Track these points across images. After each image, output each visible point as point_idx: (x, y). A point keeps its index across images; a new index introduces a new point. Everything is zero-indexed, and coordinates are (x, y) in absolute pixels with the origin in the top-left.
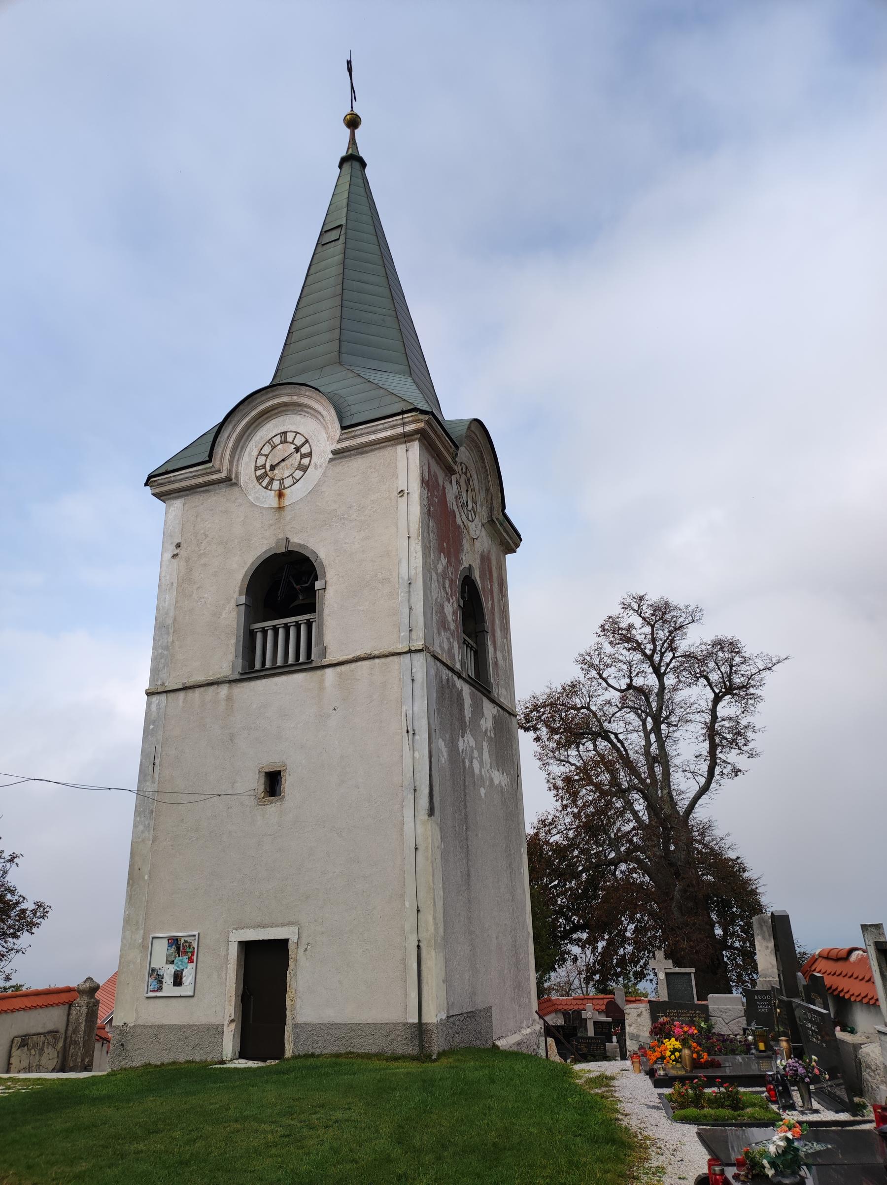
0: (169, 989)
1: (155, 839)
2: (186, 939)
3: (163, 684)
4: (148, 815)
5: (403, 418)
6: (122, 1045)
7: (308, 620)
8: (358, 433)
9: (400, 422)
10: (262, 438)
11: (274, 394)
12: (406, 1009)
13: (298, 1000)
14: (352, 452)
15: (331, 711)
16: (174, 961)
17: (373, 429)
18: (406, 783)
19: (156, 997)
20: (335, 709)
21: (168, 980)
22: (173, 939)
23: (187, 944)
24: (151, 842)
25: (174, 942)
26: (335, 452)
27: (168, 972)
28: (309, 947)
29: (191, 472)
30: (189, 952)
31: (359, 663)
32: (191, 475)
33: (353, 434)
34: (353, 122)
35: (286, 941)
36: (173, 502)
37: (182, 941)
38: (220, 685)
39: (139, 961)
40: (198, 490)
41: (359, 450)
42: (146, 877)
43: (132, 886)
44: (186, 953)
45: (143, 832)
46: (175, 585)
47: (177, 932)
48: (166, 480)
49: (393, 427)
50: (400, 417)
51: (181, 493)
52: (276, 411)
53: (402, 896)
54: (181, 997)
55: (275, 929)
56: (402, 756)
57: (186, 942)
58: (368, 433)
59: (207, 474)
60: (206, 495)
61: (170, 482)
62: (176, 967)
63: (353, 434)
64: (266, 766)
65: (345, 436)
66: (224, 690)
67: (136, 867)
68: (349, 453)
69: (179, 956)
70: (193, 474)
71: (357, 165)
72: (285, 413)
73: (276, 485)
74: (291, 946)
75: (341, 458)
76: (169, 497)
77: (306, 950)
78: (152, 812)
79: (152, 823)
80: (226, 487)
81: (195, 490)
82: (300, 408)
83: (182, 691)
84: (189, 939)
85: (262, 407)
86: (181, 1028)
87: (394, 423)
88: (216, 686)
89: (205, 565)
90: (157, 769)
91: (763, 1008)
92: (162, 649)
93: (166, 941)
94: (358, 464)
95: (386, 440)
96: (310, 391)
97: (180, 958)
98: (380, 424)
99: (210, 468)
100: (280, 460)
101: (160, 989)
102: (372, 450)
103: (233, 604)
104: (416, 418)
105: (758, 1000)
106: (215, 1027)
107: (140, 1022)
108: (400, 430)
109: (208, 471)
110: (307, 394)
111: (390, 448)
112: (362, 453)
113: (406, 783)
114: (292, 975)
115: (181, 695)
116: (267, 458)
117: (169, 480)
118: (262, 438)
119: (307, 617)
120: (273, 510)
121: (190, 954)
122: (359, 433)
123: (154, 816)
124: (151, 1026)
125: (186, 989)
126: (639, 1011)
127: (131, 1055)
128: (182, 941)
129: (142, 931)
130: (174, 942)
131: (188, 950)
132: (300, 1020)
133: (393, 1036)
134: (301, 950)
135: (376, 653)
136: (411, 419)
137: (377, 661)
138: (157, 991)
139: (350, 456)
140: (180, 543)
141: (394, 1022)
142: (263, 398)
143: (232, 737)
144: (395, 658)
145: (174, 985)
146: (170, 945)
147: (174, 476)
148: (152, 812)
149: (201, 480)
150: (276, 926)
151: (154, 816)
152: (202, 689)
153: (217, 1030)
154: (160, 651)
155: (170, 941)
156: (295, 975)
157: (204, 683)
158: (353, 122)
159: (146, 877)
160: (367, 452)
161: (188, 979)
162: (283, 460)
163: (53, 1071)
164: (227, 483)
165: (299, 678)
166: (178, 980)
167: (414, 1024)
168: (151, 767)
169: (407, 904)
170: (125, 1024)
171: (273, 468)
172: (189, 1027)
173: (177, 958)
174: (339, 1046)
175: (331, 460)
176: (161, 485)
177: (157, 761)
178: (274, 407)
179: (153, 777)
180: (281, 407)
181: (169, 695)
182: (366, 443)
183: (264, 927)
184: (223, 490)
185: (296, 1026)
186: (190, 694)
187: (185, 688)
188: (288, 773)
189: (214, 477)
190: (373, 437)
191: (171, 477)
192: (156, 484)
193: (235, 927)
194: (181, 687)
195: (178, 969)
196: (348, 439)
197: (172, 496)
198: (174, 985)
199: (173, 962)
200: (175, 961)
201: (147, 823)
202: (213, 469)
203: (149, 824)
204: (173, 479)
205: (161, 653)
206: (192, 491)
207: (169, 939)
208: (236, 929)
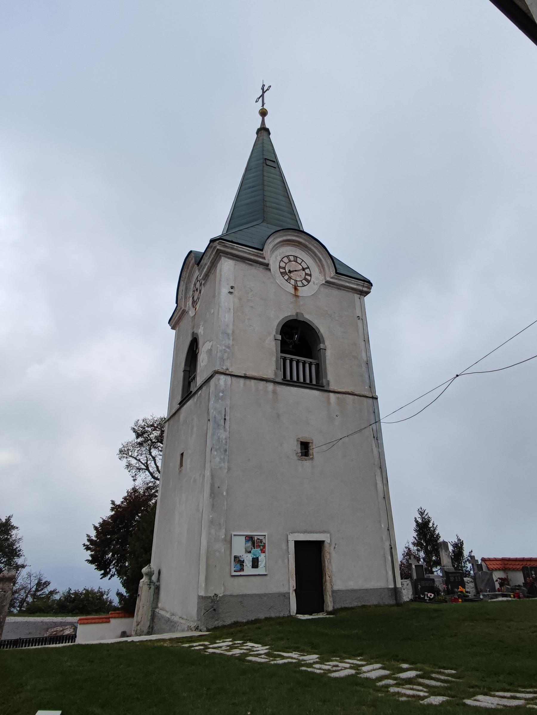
0: (248, 569)
1: (229, 469)
2: (258, 537)
3: (227, 369)
4: (223, 452)
5: (364, 283)
6: (214, 610)
7: (311, 362)
8: (343, 279)
9: (362, 284)
10: (283, 252)
11: (298, 235)
12: (388, 581)
13: (333, 577)
14: (335, 286)
15: (335, 417)
16: (250, 551)
17: (350, 281)
18: (376, 463)
19: (241, 576)
20: (337, 416)
21: (248, 563)
22: (249, 537)
23: (259, 541)
24: (226, 470)
25: (250, 539)
26: (327, 282)
27: (248, 559)
28: (336, 546)
29: (248, 250)
30: (261, 546)
31: (347, 395)
32: (248, 251)
33: (340, 278)
34: (263, 113)
35: (323, 542)
36: (228, 260)
37: (256, 539)
38: (268, 383)
39: (223, 550)
40: (247, 261)
41: (338, 287)
42: (225, 493)
43: (214, 498)
44: (259, 546)
45: (220, 463)
46: (232, 310)
47: (251, 532)
48: (231, 246)
49: (358, 285)
50: (363, 282)
51: (235, 258)
52: (294, 243)
53: (380, 521)
54: (259, 575)
55: (315, 534)
56: (372, 449)
57: (258, 539)
58: (346, 281)
59: (257, 256)
60: (250, 267)
61: (232, 248)
62: (252, 556)
63: (340, 278)
64: (301, 438)
65: (336, 277)
66: (270, 386)
67: (216, 486)
68: (333, 285)
69: (254, 548)
70: (249, 252)
71: (265, 133)
72: (297, 247)
73: (292, 282)
74: (326, 544)
75: (328, 286)
76: (226, 255)
77: (335, 548)
78: (226, 450)
79: (226, 458)
80: (263, 269)
81: (244, 261)
82: (306, 249)
83: (242, 378)
84: (260, 538)
85: (301, 240)
86: (260, 596)
87: (360, 283)
88: (265, 382)
89: (252, 307)
90: (227, 423)
91: (452, 579)
92: (225, 347)
93: (244, 537)
94: (335, 292)
95: (352, 289)
96: (317, 244)
97: (255, 549)
98: (353, 280)
99: (261, 254)
100: (294, 270)
101: (242, 569)
102: (344, 290)
103: (272, 337)
104: (369, 286)
105: (450, 576)
106: (283, 594)
107: (228, 593)
108: (361, 288)
109: (259, 255)
110: (315, 245)
111: (351, 293)
112: (338, 289)
113: (376, 463)
114: (329, 562)
115: (242, 381)
116: (286, 265)
117: (232, 247)
118: (283, 252)
119: (311, 360)
120: (292, 295)
121: (262, 547)
122: (342, 279)
123: (227, 453)
124: (237, 596)
125: (260, 570)
126: (407, 582)
127: (222, 617)
128: (256, 539)
129: (224, 530)
130: (250, 539)
131: (260, 544)
132: (336, 588)
133: (383, 595)
134: (332, 548)
135: (356, 393)
136: (366, 285)
137: (356, 397)
138: (240, 571)
139: (332, 287)
140: (233, 287)
141: (383, 587)
142: (292, 233)
143: (278, 416)
144: (365, 399)
145: (252, 567)
146: (247, 541)
147: (237, 246)
148: (226, 450)
149: (252, 257)
150: (316, 533)
151: (227, 453)
152: (256, 381)
153: (286, 596)
154: (224, 348)
155: (247, 538)
156: (330, 562)
157: (259, 378)
158: (263, 113)
159: (225, 493)
160: (340, 289)
161: (261, 564)
162: (296, 271)
163: (97, 640)
164: (265, 267)
165: (316, 393)
166: (255, 563)
167: (392, 588)
168: (222, 421)
169: (383, 526)
170: (215, 594)
171: (290, 272)
172: (265, 595)
173: (253, 549)
174: (357, 602)
175: (323, 284)
176: (226, 246)
177: (227, 418)
178: (294, 241)
179: (225, 427)
180: (296, 242)
181: (233, 378)
182: (344, 285)
183: (308, 533)
184: (261, 269)
185: (333, 592)
186: (248, 382)
187: (245, 377)
188: (314, 445)
189: (261, 260)
190: (348, 284)
191: (235, 246)
192: (223, 244)
193: (290, 531)
194: (243, 375)
195: (254, 557)
196: (336, 279)
197: (228, 256)
198: (252, 567)
199: (250, 552)
200: (252, 551)
201: (222, 457)
202: (262, 256)
203: (224, 458)
204: (235, 247)
205: (225, 350)
206: (242, 260)
207: (247, 536)
208: (292, 533)
